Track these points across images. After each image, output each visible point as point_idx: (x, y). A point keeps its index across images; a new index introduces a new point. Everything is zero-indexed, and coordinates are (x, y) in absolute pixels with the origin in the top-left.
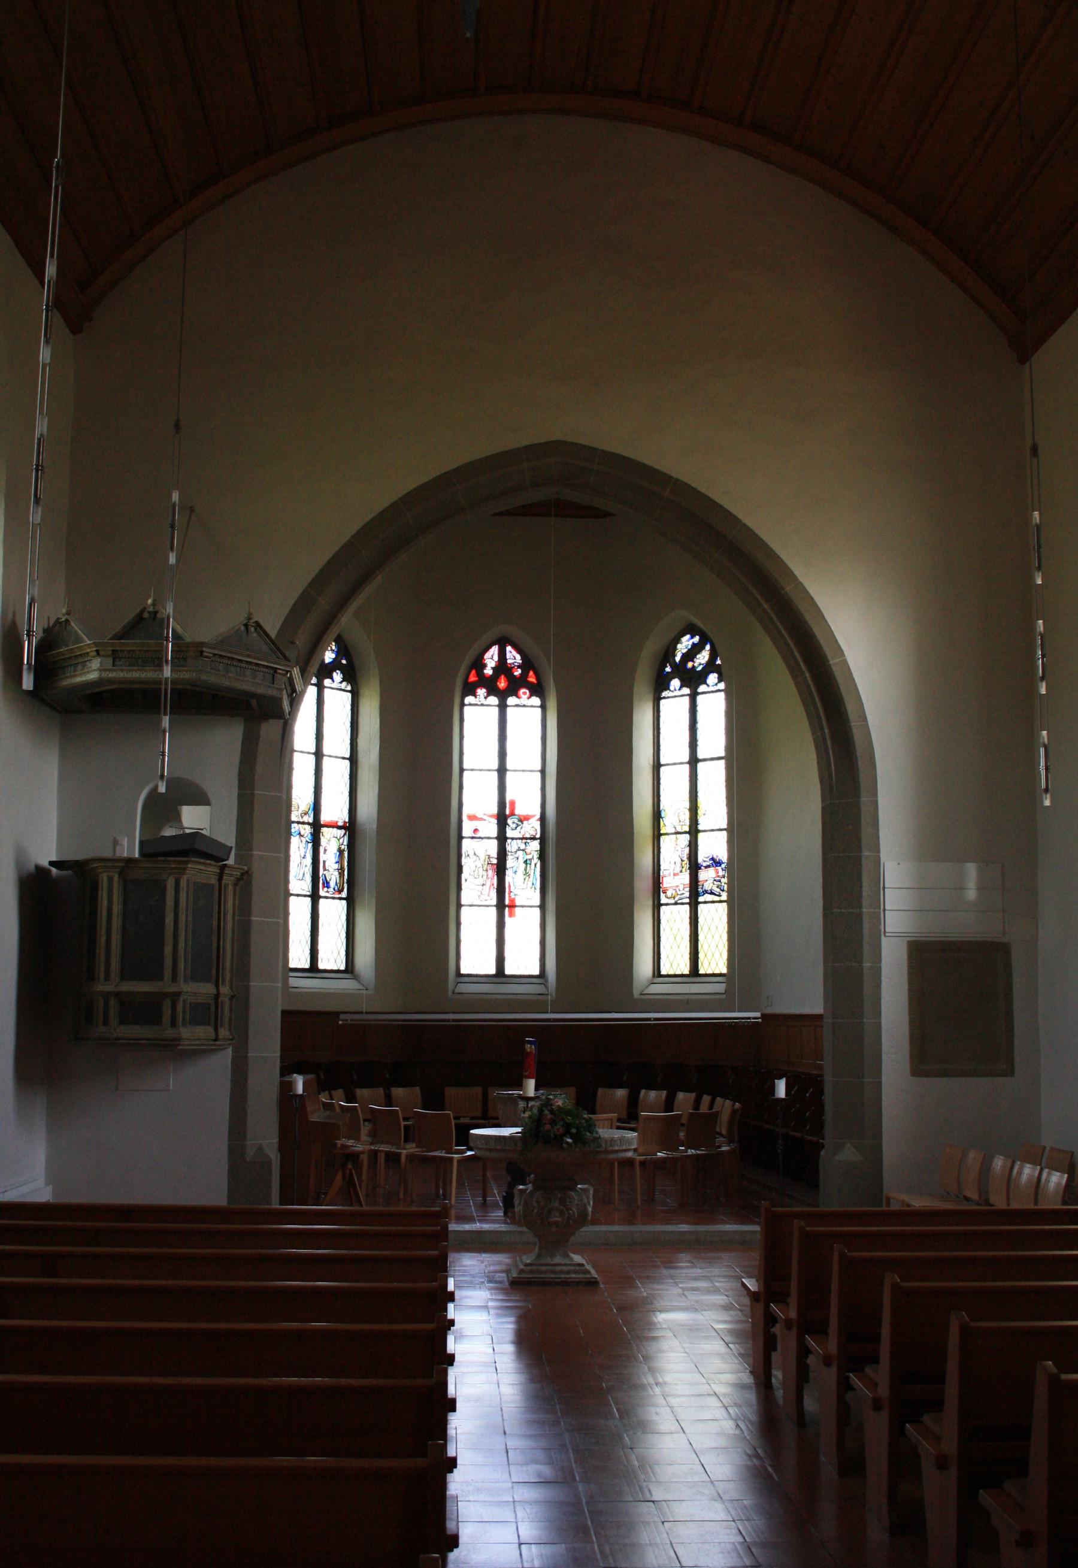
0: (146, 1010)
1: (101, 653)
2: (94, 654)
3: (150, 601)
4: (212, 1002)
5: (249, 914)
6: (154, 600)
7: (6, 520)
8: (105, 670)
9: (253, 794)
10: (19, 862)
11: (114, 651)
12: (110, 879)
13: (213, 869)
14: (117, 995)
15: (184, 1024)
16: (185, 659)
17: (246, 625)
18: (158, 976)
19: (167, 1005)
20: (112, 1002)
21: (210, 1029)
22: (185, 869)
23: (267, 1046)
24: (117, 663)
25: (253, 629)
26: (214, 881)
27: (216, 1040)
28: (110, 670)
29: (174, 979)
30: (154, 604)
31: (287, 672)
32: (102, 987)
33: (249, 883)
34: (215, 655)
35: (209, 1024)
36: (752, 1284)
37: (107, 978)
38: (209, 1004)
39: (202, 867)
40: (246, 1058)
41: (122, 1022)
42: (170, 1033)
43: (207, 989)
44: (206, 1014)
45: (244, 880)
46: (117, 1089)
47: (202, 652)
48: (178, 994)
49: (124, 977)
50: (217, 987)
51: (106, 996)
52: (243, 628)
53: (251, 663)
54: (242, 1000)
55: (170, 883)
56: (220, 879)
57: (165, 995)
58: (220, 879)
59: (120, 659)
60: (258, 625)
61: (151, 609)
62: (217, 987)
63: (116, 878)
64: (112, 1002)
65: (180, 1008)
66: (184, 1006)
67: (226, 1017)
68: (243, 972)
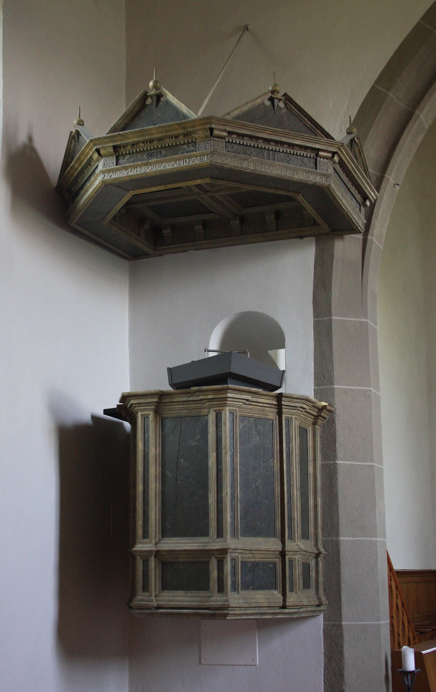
0: (189, 572)
1: (102, 152)
2: (96, 156)
3: (151, 84)
4: (278, 561)
5: (335, 458)
6: (156, 82)
7: (4, 33)
8: (109, 171)
9: (331, 320)
10: (54, 409)
11: (115, 147)
12: (145, 418)
13: (266, 400)
14: (158, 554)
15: (235, 588)
16: (194, 143)
17: (271, 99)
18: (204, 533)
19: (214, 564)
20: (152, 563)
21: (277, 594)
22: (225, 399)
23: (370, 614)
24: (121, 161)
25: (282, 105)
26: (272, 414)
27: (284, 607)
28: (112, 171)
29: (220, 533)
30: (155, 87)
31: (334, 153)
32: (142, 546)
33: (332, 422)
34: (230, 133)
35: (276, 588)
36: (304, 212)
37: (146, 535)
38: (275, 564)
39: (249, 397)
40: (340, 627)
41: (165, 587)
42: (216, 600)
43: (266, 546)
44: (270, 575)
45: (322, 416)
46: (200, 663)
47: (212, 130)
48: (224, 551)
49: (165, 533)
50: (283, 542)
51: (146, 556)
52: (268, 103)
53: (282, 143)
54: (330, 556)
55: (212, 418)
56: (280, 413)
57: (209, 553)
58: (280, 413)
59: (124, 155)
60: (287, 99)
61: (153, 92)
62: (283, 542)
63: (151, 417)
64: (152, 563)
65: (228, 567)
66: (234, 567)
67: (327, 580)
68: (332, 526)
